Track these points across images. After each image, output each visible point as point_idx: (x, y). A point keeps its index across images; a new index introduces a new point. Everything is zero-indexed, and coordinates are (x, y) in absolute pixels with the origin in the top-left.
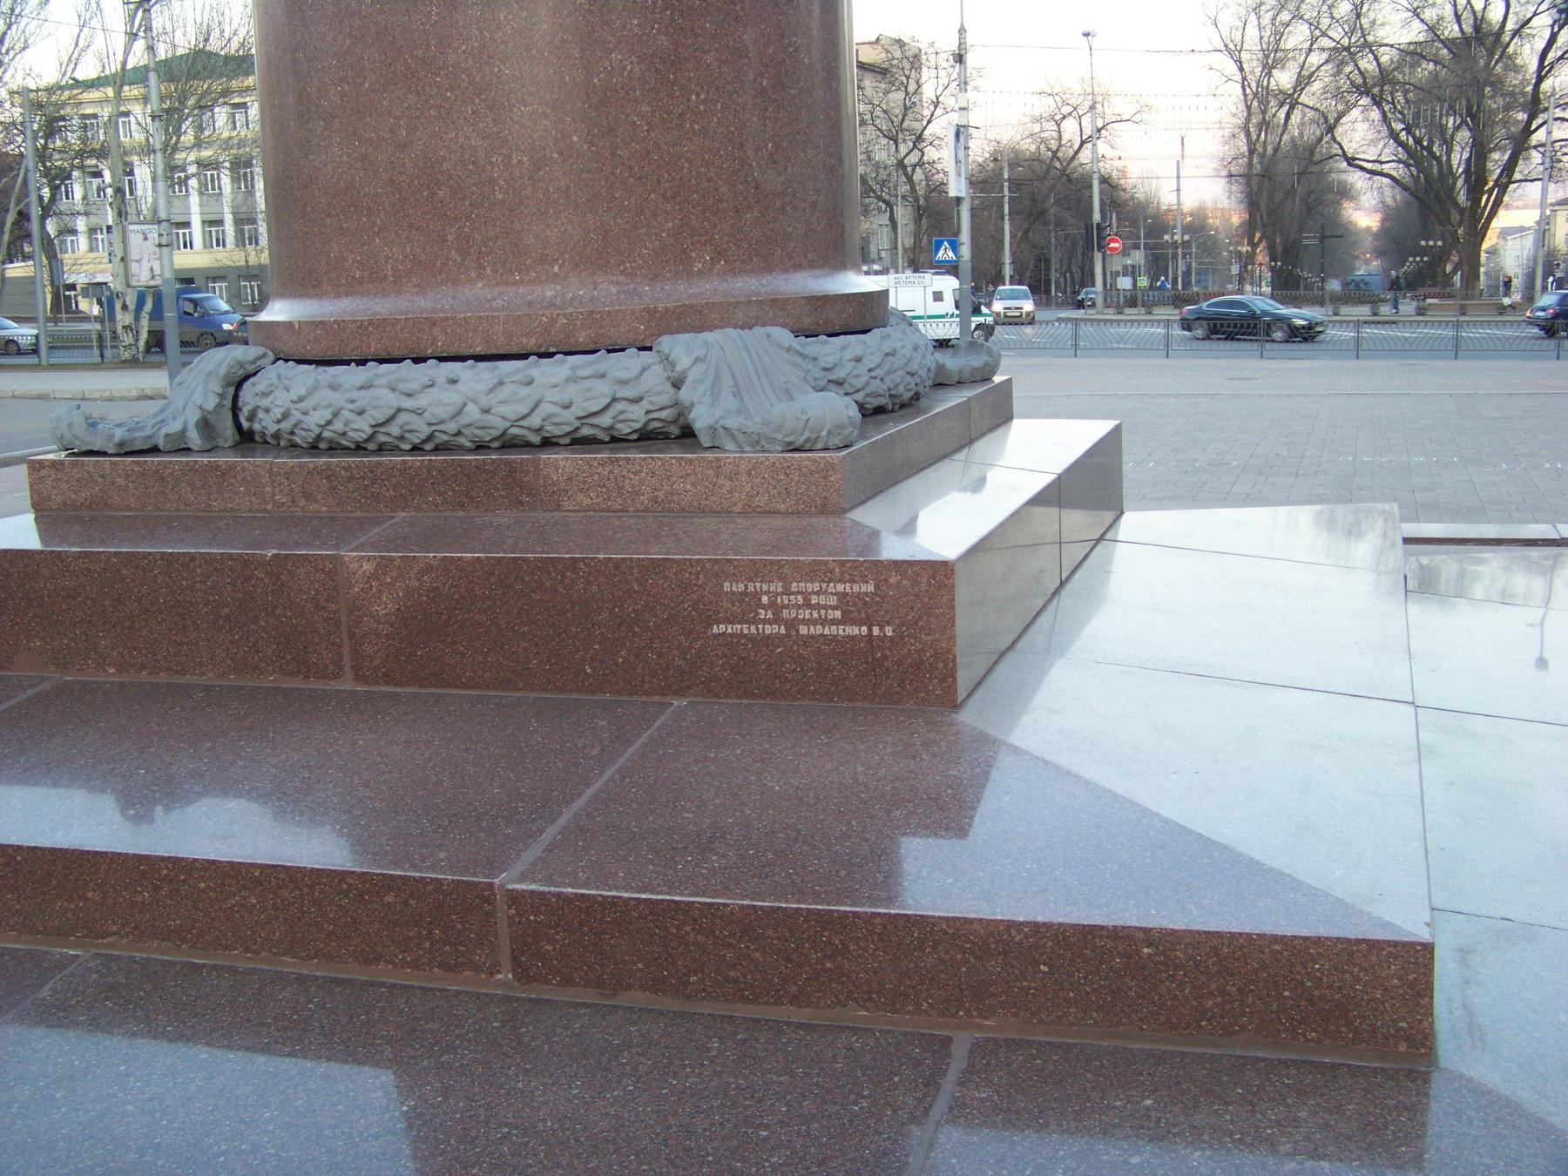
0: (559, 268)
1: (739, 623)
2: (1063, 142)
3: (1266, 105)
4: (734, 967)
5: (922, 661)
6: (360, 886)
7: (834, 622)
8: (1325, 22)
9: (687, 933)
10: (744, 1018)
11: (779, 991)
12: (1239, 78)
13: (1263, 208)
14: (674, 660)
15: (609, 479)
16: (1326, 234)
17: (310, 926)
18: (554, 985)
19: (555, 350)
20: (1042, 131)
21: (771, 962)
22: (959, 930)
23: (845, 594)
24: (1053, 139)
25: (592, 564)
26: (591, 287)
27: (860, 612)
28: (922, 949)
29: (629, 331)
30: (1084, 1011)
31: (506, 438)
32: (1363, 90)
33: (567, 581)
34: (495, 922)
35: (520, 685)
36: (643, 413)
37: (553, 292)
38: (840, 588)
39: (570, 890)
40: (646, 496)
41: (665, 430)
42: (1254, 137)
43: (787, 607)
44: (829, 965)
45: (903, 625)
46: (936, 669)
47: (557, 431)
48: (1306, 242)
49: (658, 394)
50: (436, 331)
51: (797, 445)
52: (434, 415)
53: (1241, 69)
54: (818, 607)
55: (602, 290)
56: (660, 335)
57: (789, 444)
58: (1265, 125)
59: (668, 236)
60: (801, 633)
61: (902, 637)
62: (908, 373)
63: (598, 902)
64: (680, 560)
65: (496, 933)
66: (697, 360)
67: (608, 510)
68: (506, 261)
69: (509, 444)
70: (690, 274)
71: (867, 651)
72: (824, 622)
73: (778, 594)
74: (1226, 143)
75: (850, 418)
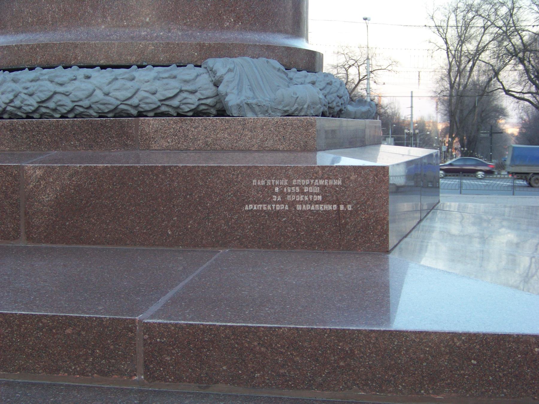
0: (150, 19)
1: (261, 204)
2: (349, 80)
3: (460, 62)
4: (283, 366)
5: (368, 224)
6: (50, 324)
7: (317, 202)
8: (492, 18)
9: (255, 347)
10: (288, 398)
11: (310, 381)
12: (445, 47)
13: (457, 119)
14: (221, 226)
15: (179, 131)
16: (493, 131)
17: (16, 350)
18: (170, 382)
19: (146, 64)
20: (338, 73)
21: (306, 363)
22: (422, 339)
23: (324, 186)
24: (344, 78)
25: (175, 169)
26: (167, 31)
27: (333, 197)
28: (400, 352)
29: (189, 55)
30: (498, 388)
31: (117, 111)
32: (513, 54)
33: (159, 180)
34: (135, 344)
35: (128, 242)
36: (197, 100)
37: (146, 33)
38: (321, 182)
39: (183, 322)
40: (201, 141)
41: (208, 111)
42: (453, 79)
43: (290, 194)
44: (342, 364)
45: (358, 203)
46: (377, 229)
47: (147, 108)
48: (482, 135)
49: (206, 89)
50: (77, 51)
51: (290, 112)
52: (75, 96)
53: (446, 43)
54: (308, 193)
55: (173, 33)
56: (206, 59)
57: (286, 111)
58: (460, 72)
59: (211, 5)
60: (298, 209)
61: (357, 211)
62: (338, 96)
63: (200, 329)
64: (227, 167)
65: (135, 351)
66: (230, 70)
67: (179, 149)
68: (119, 14)
69: (118, 113)
70: (222, 28)
71: (336, 219)
72: (311, 202)
73: (285, 186)
74: (437, 83)
75: (320, 99)
